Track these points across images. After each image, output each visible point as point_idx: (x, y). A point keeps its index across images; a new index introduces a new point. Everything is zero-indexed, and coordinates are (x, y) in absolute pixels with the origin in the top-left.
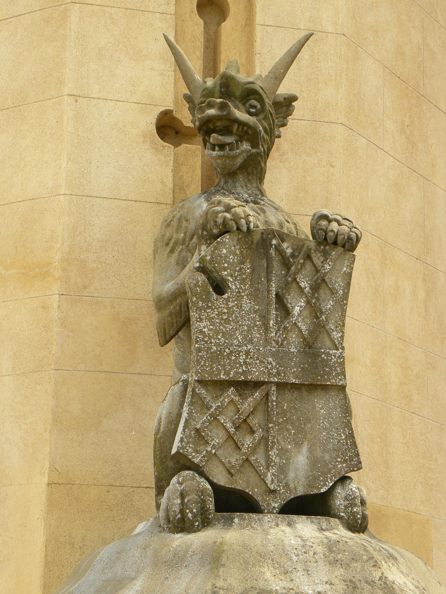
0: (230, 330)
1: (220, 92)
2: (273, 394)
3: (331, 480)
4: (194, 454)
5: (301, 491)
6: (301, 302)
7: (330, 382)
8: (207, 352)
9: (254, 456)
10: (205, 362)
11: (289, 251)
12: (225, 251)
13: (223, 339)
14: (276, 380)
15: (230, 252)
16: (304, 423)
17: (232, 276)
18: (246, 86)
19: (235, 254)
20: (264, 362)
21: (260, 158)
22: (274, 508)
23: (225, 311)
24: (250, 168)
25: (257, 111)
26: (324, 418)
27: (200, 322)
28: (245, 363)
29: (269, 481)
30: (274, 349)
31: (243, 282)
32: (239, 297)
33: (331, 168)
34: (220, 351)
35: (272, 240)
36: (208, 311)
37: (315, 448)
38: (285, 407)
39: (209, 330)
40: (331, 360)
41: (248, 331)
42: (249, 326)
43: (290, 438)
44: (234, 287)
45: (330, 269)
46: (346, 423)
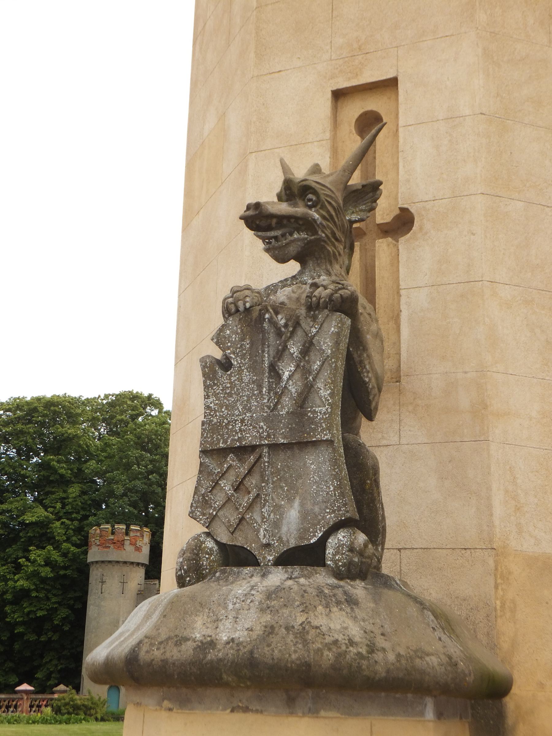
0: (233, 402)
1: (286, 194)
2: (265, 456)
3: (320, 530)
4: (201, 517)
5: (293, 543)
6: (291, 367)
7: (315, 437)
8: (209, 425)
9: (249, 515)
10: (207, 434)
11: (283, 322)
12: (228, 332)
13: (226, 411)
14: (266, 442)
15: (233, 332)
16: (296, 479)
17: (234, 353)
18: (300, 184)
19: (237, 333)
20: (256, 427)
21: (322, 243)
22: (269, 560)
23: (229, 385)
24: (316, 254)
25: (313, 203)
26: (314, 473)
27: (207, 399)
28: (240, 430)
29: (261, 537)
30: (265, 414)
31: (243, 357)
32: (240, 371)
33: (472, 237)
34: (220, 422)
35: (265, 314)
36: (214, 388)
37: (305, 502)
38: (279, 467)
39: (215, 405)
40: (317, 417)
41: (248, 401)
42: (248, 396)
43: (283, 495)
44: (236, 363)
45: (318, 331)
46: (335, 475)
